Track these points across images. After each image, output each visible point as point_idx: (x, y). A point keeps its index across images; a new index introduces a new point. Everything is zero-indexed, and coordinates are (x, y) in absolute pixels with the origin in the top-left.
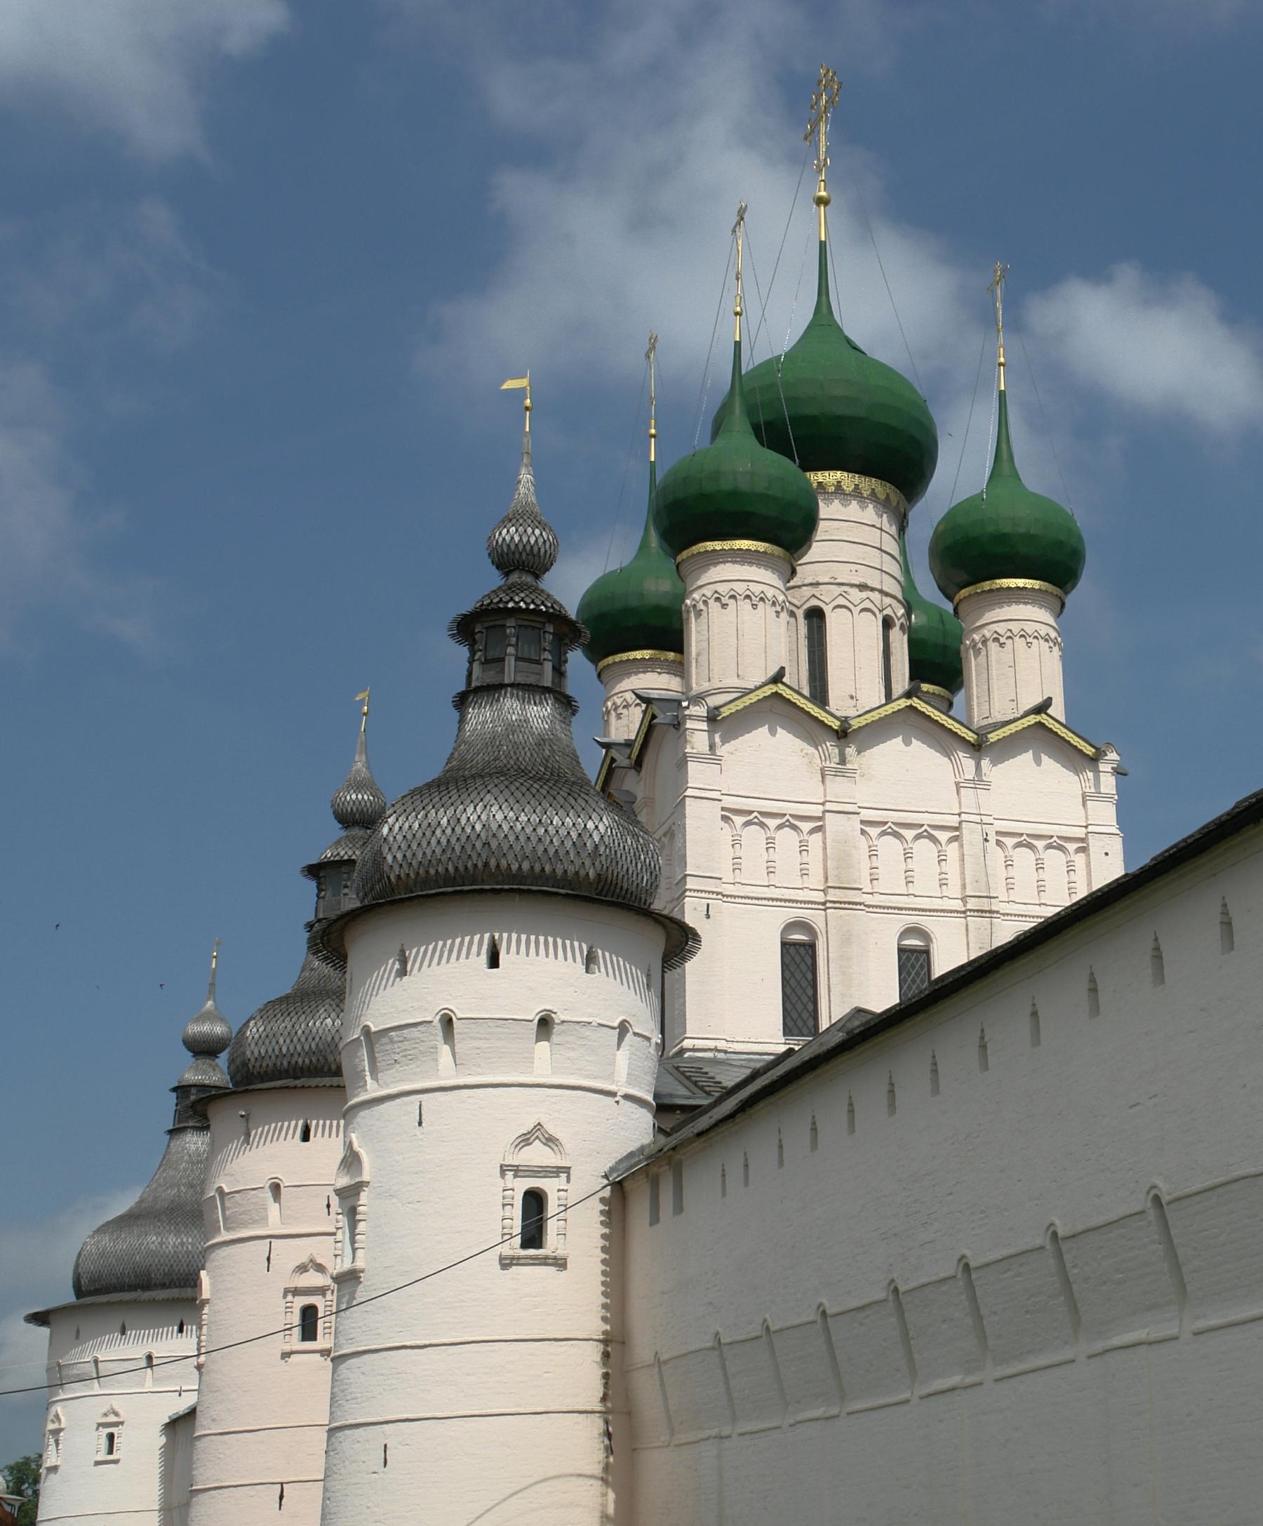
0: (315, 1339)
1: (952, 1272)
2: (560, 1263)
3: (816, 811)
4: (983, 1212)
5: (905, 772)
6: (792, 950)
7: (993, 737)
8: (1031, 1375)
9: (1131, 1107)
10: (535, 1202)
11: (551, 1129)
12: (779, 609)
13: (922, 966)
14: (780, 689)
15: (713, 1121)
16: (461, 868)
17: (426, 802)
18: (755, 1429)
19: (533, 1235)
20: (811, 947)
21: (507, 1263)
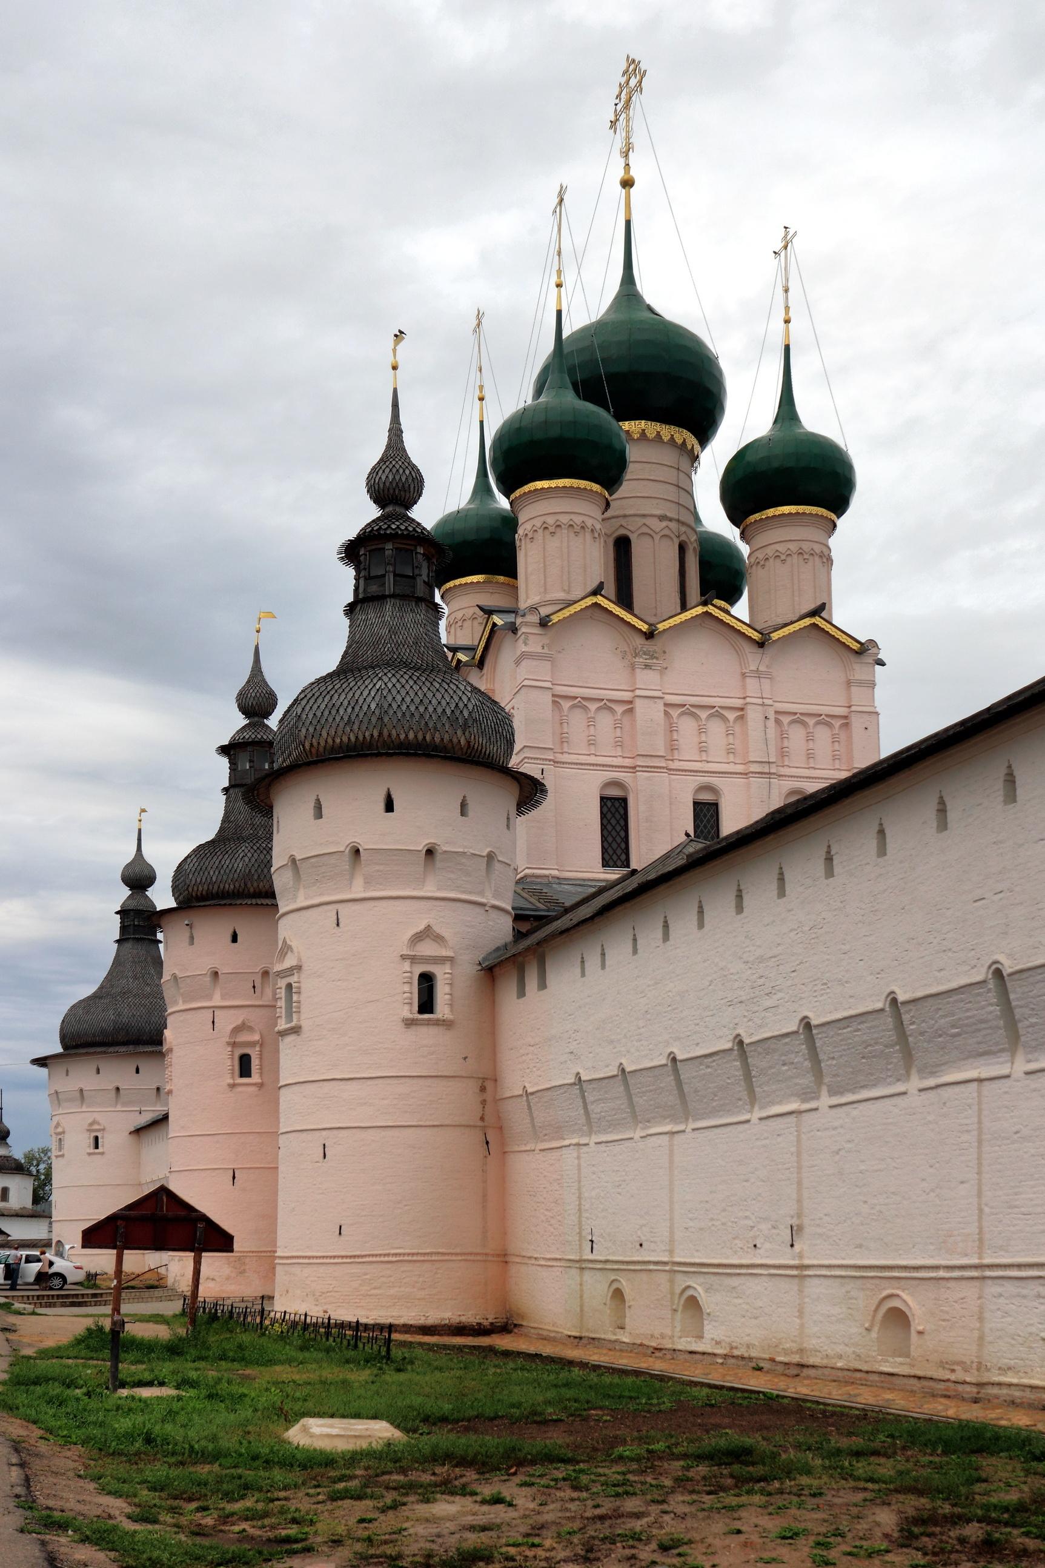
0: (250, 1076)
1: (795, 1028)
2: (447, 1024)
3: (627, 696)
4: (825, 984)
5: (700, 668)
6: (609, 804)
7: (775, 636)
8: (864, 1104)
9: (975, 901)
10: (427, 982)
11: (437, 929)
12: (596, 535)
13: (712, 816)
14: (599, 599)
15: (575, 921)
16: (361, 738)
17: (329, 688)
18: (610, 1139)
19: (426, 1005)
20: (624, 801)
21: (409, 1023)
